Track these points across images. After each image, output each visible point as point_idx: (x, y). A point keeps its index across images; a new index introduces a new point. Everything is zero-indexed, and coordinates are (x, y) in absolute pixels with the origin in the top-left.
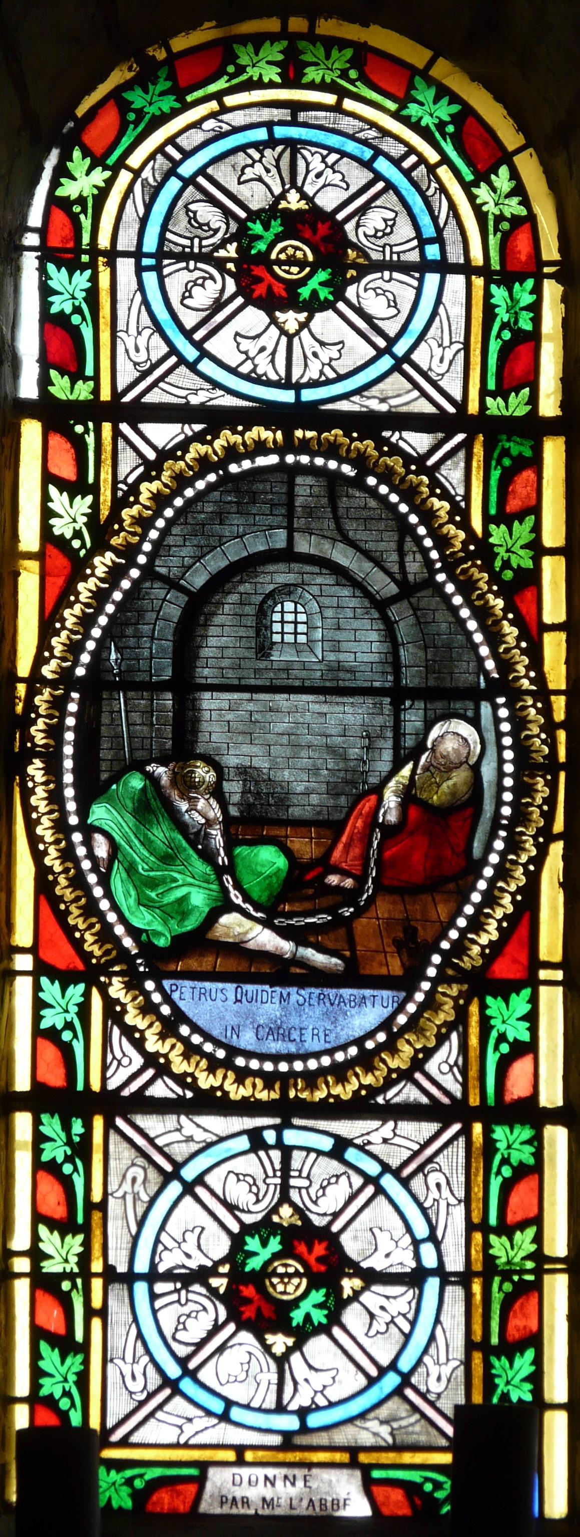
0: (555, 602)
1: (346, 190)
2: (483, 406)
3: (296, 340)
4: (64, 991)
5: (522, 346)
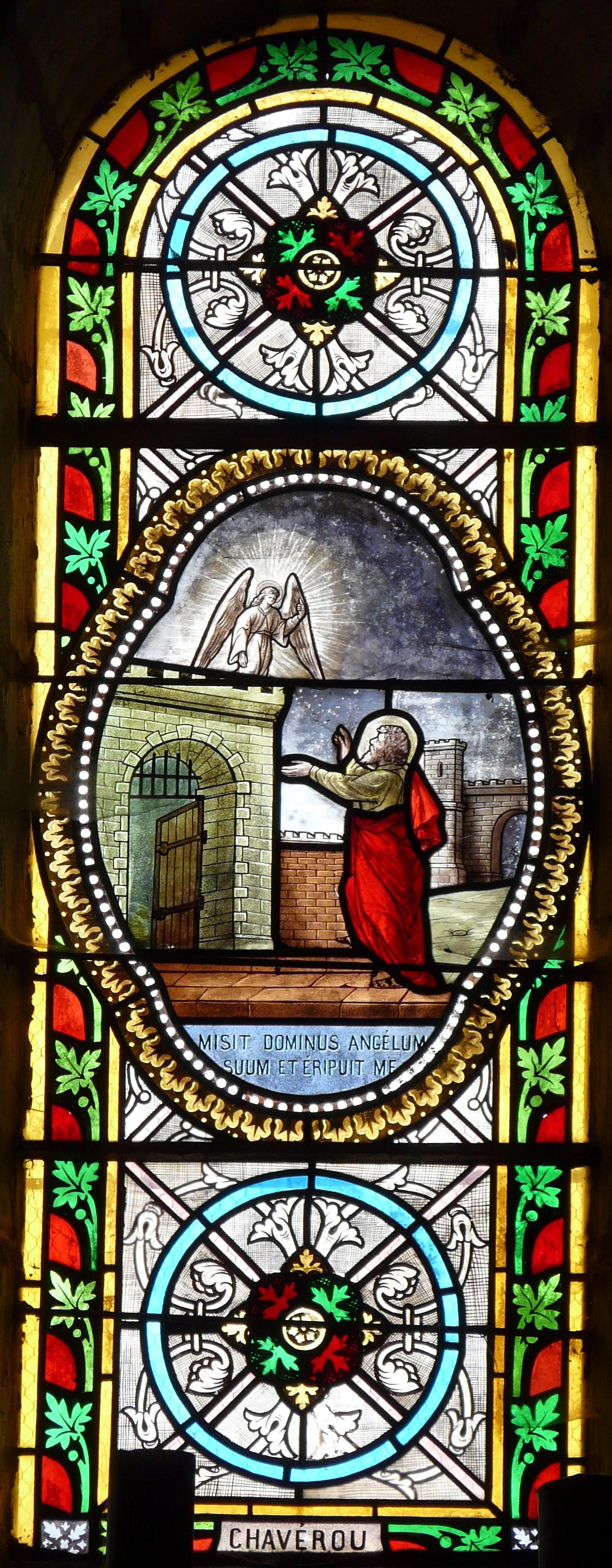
0: (590, 301)
1: (361, 1246)
2: (517, 414)
3: (323, 352)
5: (557, 353)
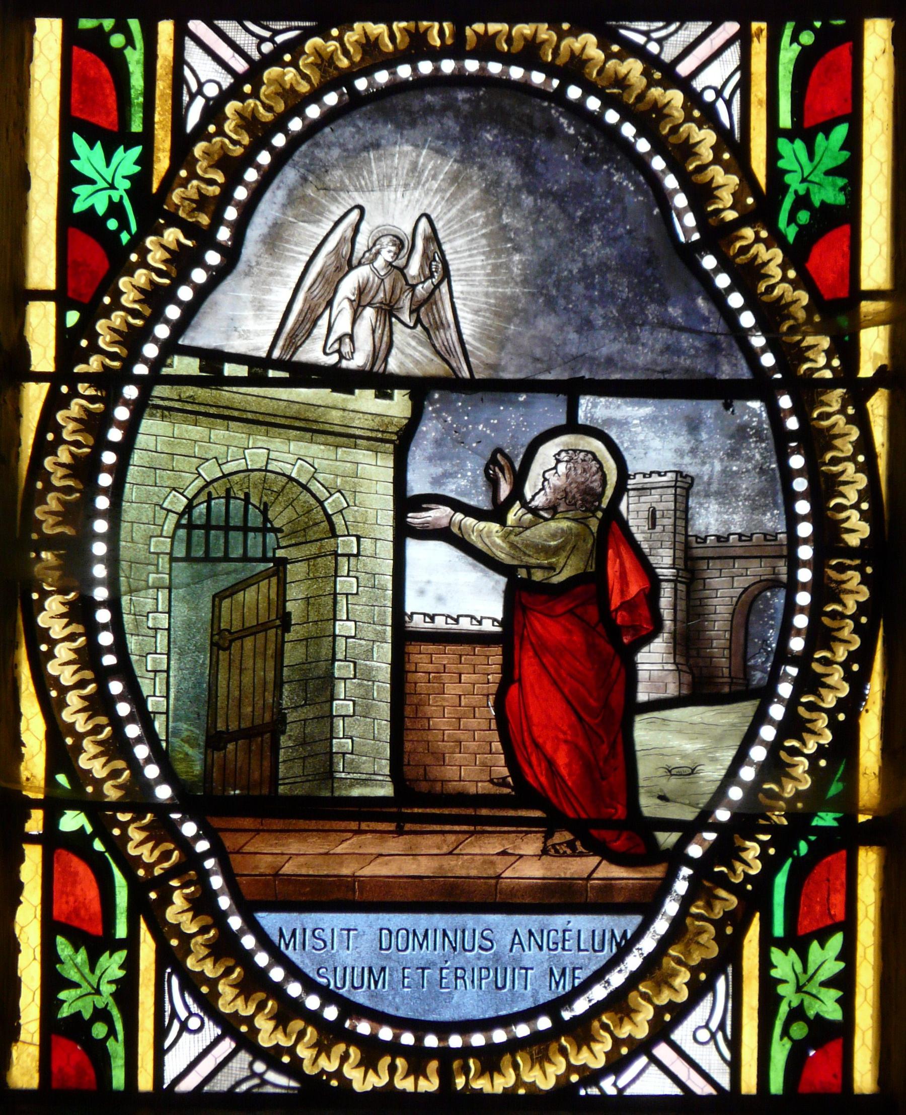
4: (93, 962)
